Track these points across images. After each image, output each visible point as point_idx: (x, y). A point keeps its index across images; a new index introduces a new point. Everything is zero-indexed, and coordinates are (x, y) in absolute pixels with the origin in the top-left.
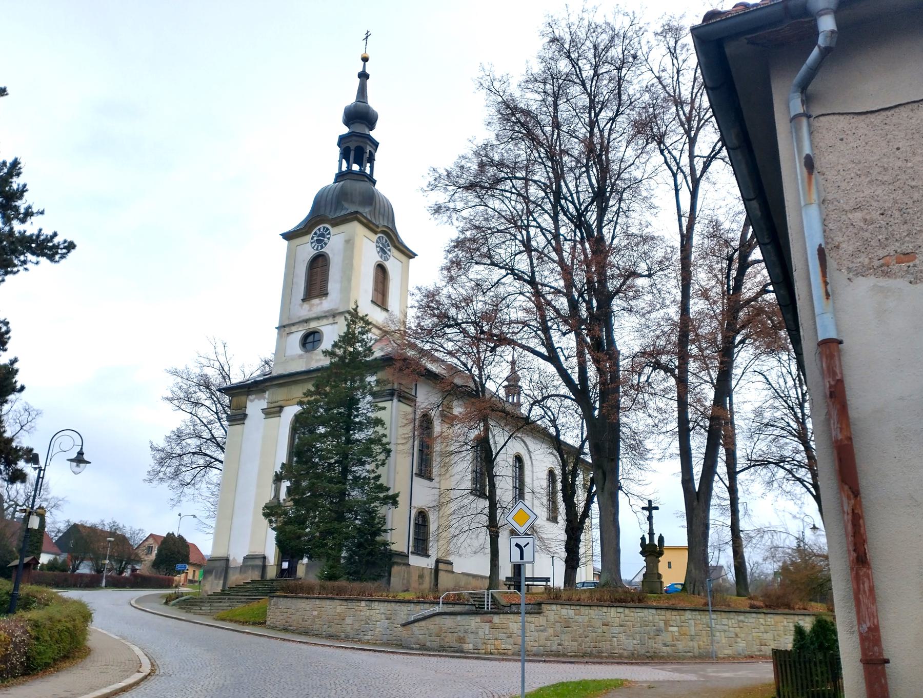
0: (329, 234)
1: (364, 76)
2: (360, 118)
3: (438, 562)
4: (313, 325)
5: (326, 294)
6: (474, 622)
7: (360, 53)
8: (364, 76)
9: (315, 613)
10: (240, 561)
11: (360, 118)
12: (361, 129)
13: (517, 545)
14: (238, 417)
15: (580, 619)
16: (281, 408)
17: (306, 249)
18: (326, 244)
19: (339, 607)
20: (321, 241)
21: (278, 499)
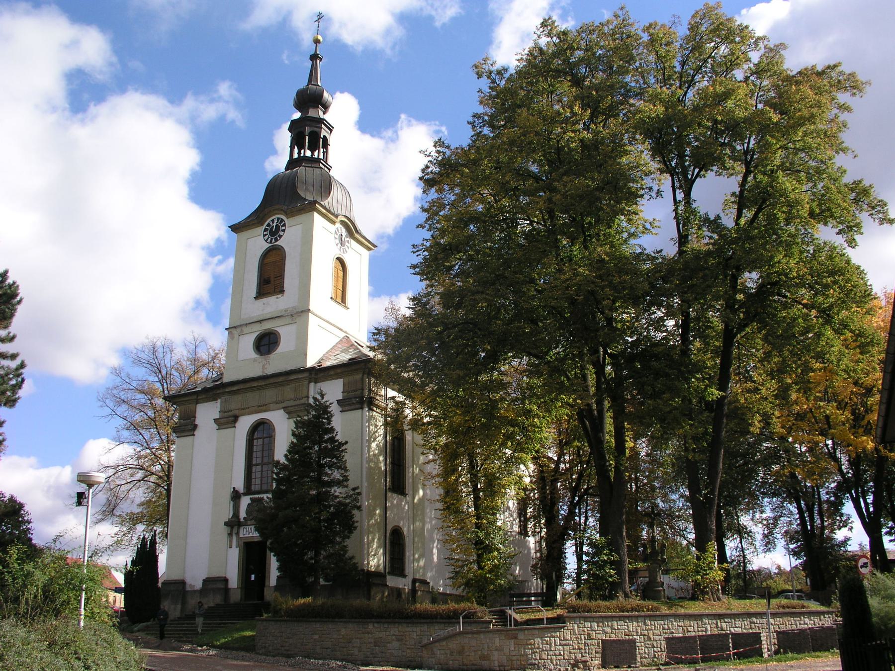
0: (284, 225)
1: (314, 57)
3: (414, 581)
4: (267, 326)
5: (282, 291)
9: (316, 637)
10: (199, 585)
14: (186, 427)
16: (236, 418)
17: (257, 243)
18: (281, 236)
19: (343, 630)
20: (275, 233)
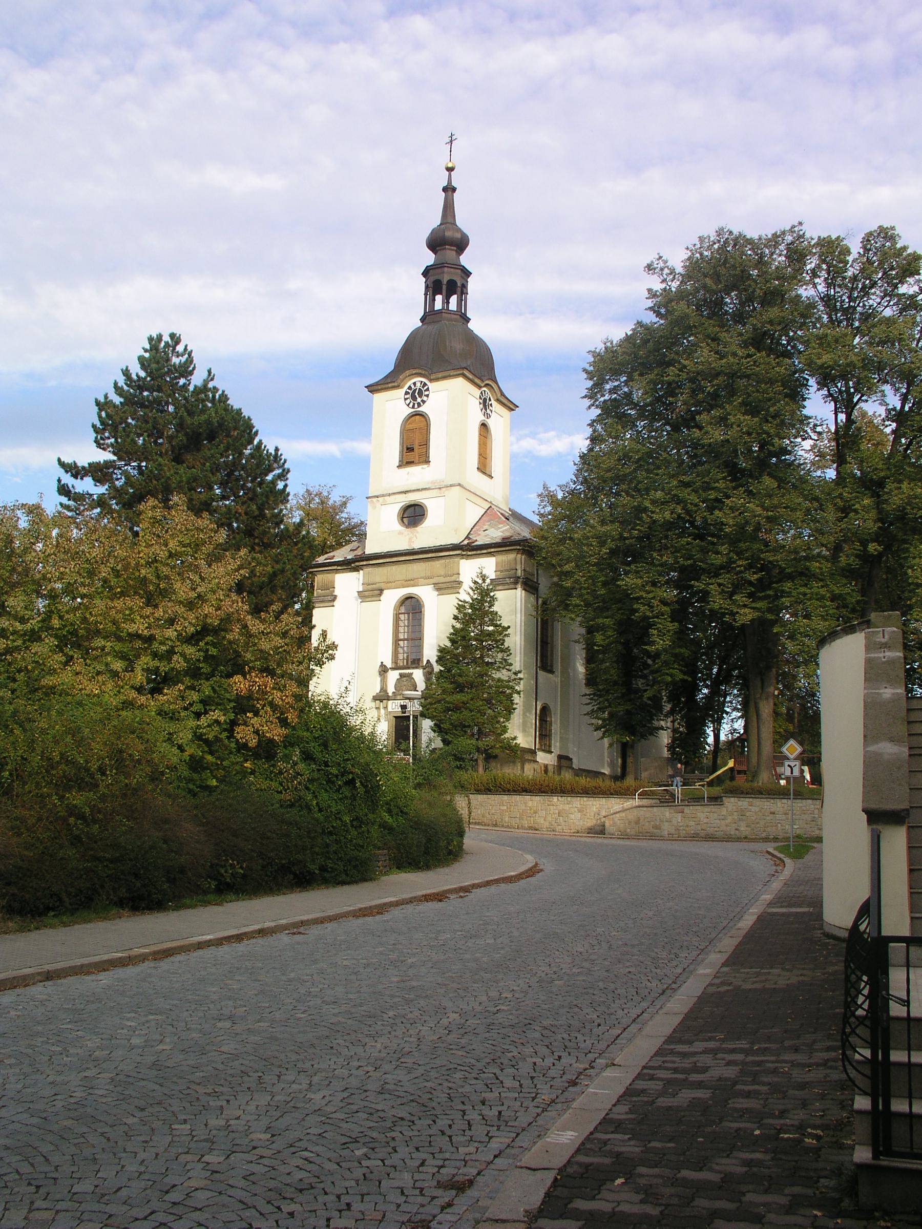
0: (428, 390)
1: (449, 190)
2: (447, 242)
6: (667, 813)
7: (445, 162)
8: (449, 190)
11: (447, 242)
12: (449, 254)
13: (789, 766)
15: (753, 809)
16: (381, 591)
20: (416, 396)
21: (386, 691)
